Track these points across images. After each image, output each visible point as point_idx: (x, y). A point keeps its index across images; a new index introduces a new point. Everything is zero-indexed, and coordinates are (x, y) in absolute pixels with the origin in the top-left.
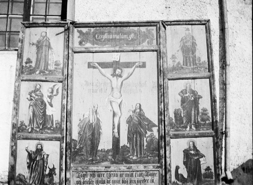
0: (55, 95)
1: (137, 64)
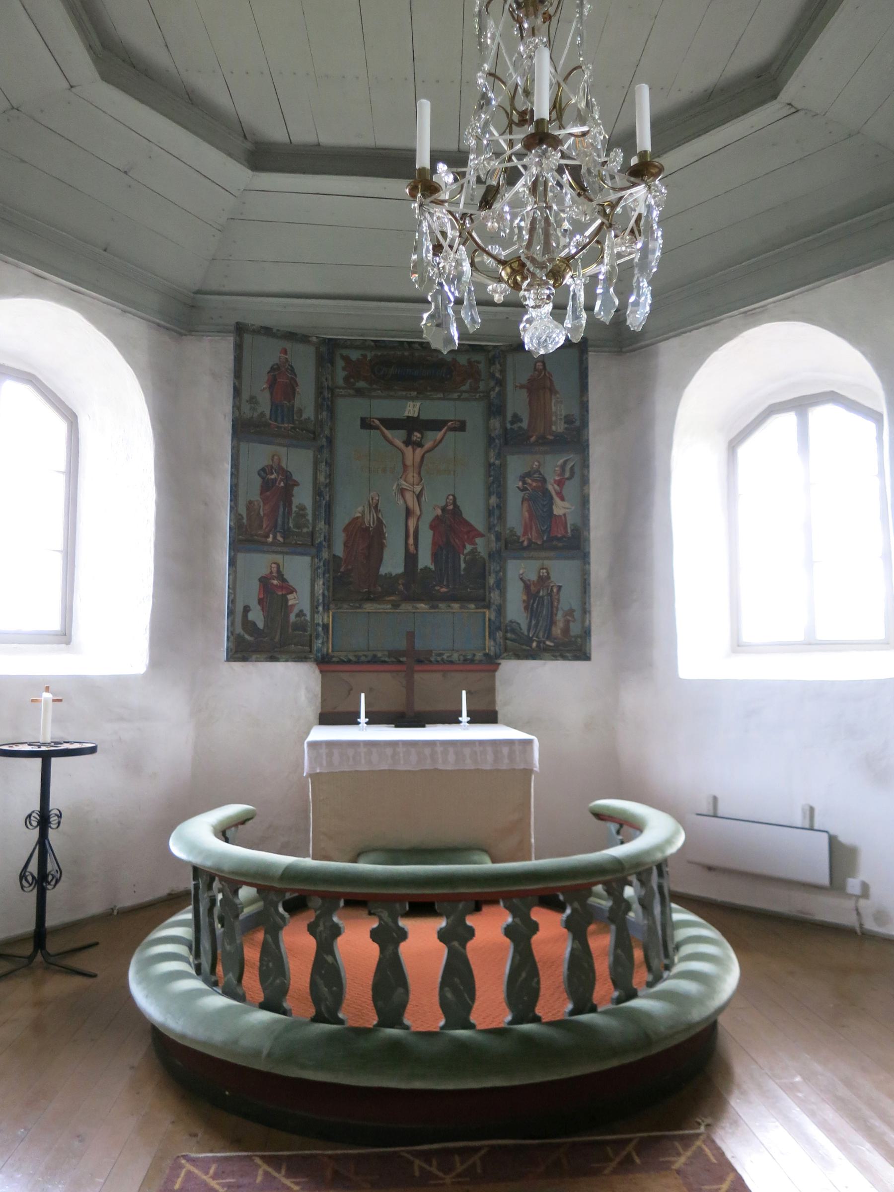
0: (568, 479)
1: (450, 424)
